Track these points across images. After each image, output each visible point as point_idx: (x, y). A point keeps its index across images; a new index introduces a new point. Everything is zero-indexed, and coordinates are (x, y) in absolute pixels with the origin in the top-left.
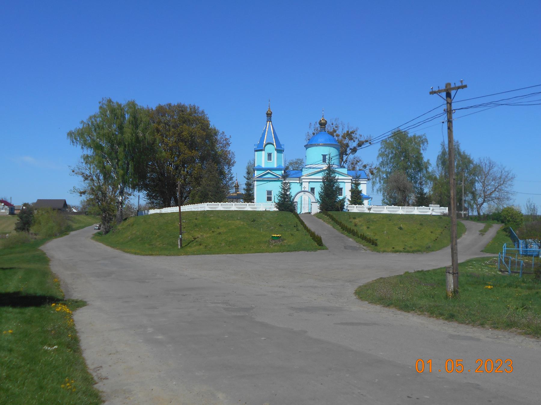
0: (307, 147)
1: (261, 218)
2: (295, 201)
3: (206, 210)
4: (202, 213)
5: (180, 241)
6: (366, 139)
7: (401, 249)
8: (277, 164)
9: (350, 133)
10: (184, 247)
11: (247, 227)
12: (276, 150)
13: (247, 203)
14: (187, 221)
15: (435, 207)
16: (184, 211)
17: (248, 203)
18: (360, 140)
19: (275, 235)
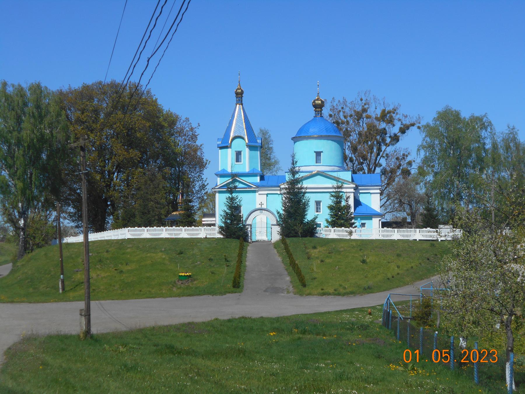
0: (296, 139)
2: (248, 222)
3: (126, 238)
4: (118, 243)
5: (61, 283)
6: (413, 121)
7: (331, 291)
9: (386, 112)
10: (69, 291)
14: (94, 255)
15: (446, 229)
16: (97, 240)
17: (146, 227)
18: (404, 123)
19: (183, 274)
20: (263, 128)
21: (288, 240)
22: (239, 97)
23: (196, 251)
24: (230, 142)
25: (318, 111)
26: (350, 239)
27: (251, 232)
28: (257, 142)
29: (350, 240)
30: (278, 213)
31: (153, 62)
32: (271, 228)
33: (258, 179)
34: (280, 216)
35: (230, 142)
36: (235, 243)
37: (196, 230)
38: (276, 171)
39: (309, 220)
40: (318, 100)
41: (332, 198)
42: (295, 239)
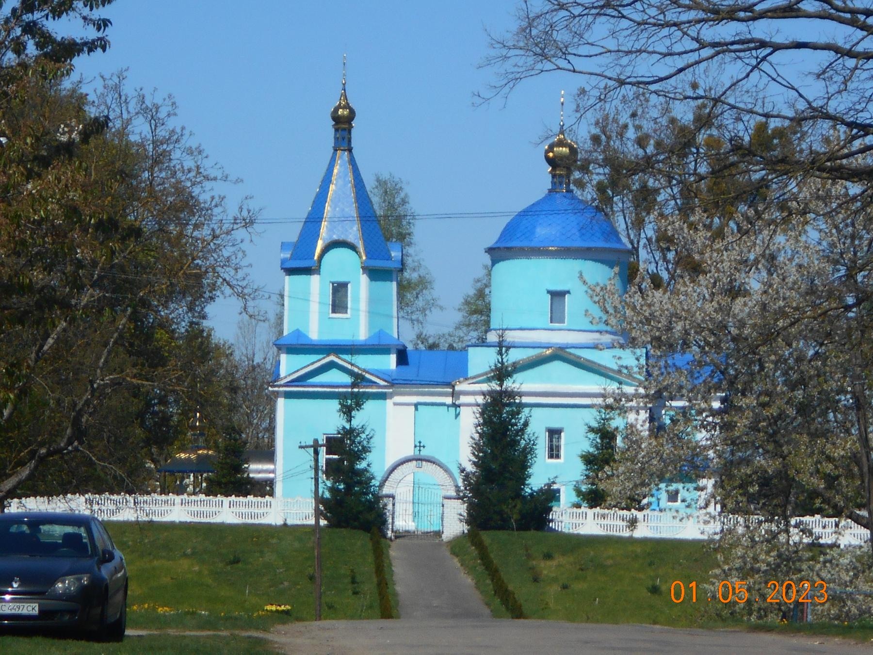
1: (261, 552)
2: (386, 490)
8: (371, 324)
11: (210, 581)
12: (367, 270)
13: (175, 497)
17: (227, 496)
19: (274, 608)
20: (385, 176)
21: (486, 537)
22: (344, 129)
23: (269, 557)
24: (316, 258)
25: (561, 176)
26: (631, 538)
27: (393, 514)
28: (389, 258)
29: (631, 540)
30: (463, 470)
31: (411, 381)
32: (443, 506)
33: (392, 360)
34: (467, 478)
35: (316, 258)
36: (360, 541)
37: (258, 505)
38: (423, 311)
39: (535, 489)
40: (561, 143)
41: (592, 436)
42: (502, 535)
